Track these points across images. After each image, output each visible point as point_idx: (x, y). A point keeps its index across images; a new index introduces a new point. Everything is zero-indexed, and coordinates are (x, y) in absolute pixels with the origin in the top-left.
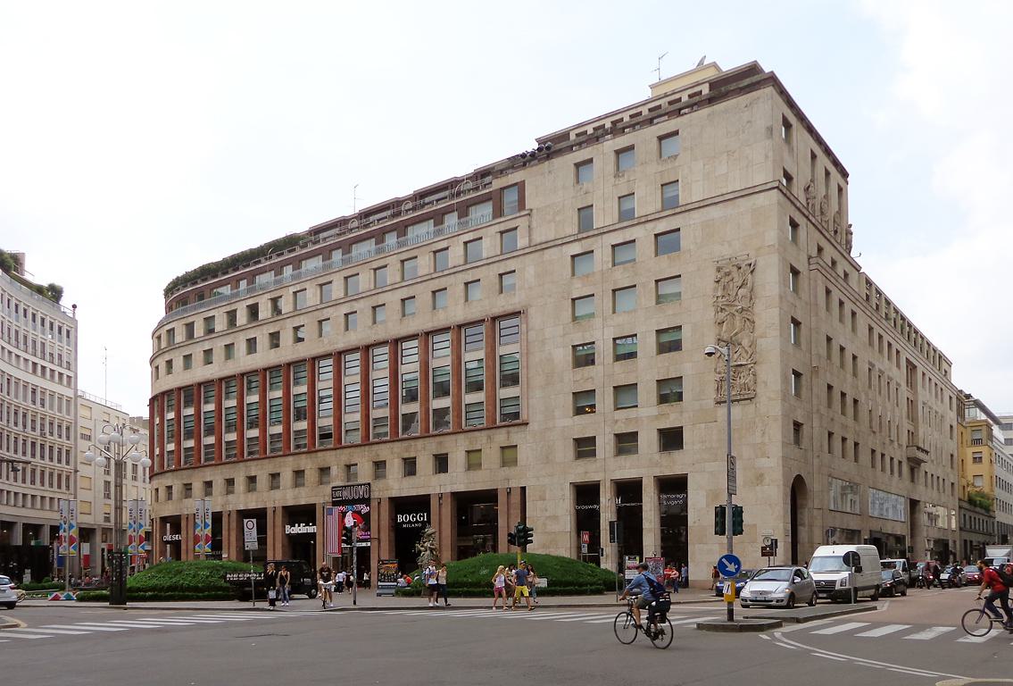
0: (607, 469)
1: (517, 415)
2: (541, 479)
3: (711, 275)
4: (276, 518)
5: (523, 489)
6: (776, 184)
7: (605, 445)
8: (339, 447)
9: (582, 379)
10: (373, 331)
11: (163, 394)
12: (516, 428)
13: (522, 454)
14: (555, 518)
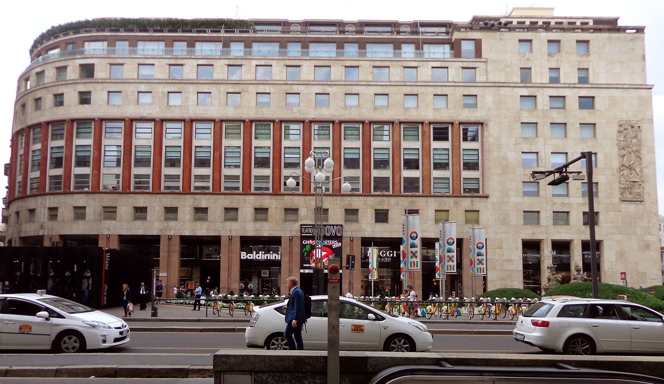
0: (548, 232)
1: (477, 191)
2: (499, 234)
3: (615, 127)
7: (546, 217)
8: (96, 191)
12: (478, 199)
13: (484, 216)
14: (510, 261)
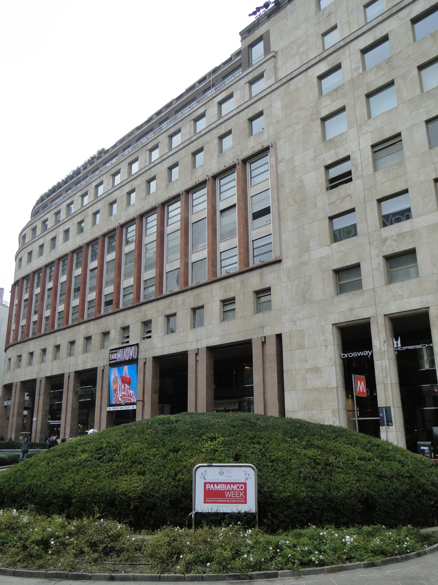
2: (298, 322)
5: (279, 337)
7: (373, 270)
9: (337, 200)
10: (146, 201)
11: (23, 278)
14: (316, 370)
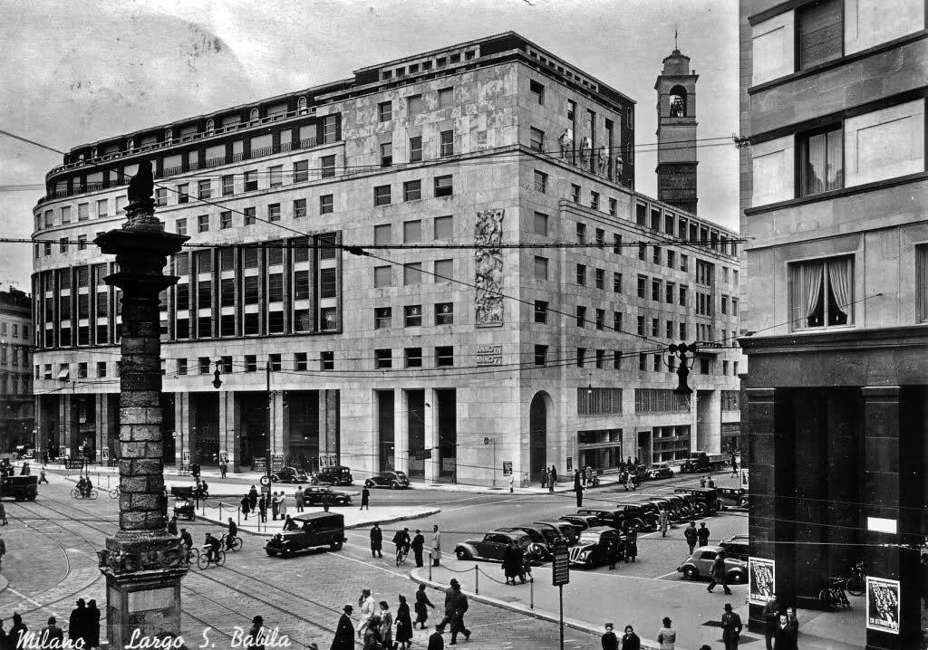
4: (229, 409)
5: (338, 392)
6: (517, 147)
